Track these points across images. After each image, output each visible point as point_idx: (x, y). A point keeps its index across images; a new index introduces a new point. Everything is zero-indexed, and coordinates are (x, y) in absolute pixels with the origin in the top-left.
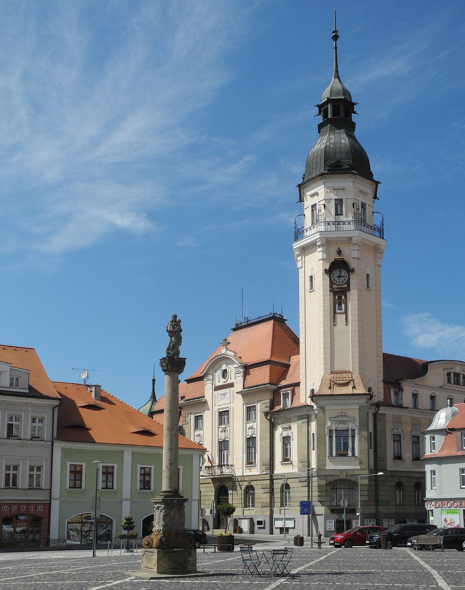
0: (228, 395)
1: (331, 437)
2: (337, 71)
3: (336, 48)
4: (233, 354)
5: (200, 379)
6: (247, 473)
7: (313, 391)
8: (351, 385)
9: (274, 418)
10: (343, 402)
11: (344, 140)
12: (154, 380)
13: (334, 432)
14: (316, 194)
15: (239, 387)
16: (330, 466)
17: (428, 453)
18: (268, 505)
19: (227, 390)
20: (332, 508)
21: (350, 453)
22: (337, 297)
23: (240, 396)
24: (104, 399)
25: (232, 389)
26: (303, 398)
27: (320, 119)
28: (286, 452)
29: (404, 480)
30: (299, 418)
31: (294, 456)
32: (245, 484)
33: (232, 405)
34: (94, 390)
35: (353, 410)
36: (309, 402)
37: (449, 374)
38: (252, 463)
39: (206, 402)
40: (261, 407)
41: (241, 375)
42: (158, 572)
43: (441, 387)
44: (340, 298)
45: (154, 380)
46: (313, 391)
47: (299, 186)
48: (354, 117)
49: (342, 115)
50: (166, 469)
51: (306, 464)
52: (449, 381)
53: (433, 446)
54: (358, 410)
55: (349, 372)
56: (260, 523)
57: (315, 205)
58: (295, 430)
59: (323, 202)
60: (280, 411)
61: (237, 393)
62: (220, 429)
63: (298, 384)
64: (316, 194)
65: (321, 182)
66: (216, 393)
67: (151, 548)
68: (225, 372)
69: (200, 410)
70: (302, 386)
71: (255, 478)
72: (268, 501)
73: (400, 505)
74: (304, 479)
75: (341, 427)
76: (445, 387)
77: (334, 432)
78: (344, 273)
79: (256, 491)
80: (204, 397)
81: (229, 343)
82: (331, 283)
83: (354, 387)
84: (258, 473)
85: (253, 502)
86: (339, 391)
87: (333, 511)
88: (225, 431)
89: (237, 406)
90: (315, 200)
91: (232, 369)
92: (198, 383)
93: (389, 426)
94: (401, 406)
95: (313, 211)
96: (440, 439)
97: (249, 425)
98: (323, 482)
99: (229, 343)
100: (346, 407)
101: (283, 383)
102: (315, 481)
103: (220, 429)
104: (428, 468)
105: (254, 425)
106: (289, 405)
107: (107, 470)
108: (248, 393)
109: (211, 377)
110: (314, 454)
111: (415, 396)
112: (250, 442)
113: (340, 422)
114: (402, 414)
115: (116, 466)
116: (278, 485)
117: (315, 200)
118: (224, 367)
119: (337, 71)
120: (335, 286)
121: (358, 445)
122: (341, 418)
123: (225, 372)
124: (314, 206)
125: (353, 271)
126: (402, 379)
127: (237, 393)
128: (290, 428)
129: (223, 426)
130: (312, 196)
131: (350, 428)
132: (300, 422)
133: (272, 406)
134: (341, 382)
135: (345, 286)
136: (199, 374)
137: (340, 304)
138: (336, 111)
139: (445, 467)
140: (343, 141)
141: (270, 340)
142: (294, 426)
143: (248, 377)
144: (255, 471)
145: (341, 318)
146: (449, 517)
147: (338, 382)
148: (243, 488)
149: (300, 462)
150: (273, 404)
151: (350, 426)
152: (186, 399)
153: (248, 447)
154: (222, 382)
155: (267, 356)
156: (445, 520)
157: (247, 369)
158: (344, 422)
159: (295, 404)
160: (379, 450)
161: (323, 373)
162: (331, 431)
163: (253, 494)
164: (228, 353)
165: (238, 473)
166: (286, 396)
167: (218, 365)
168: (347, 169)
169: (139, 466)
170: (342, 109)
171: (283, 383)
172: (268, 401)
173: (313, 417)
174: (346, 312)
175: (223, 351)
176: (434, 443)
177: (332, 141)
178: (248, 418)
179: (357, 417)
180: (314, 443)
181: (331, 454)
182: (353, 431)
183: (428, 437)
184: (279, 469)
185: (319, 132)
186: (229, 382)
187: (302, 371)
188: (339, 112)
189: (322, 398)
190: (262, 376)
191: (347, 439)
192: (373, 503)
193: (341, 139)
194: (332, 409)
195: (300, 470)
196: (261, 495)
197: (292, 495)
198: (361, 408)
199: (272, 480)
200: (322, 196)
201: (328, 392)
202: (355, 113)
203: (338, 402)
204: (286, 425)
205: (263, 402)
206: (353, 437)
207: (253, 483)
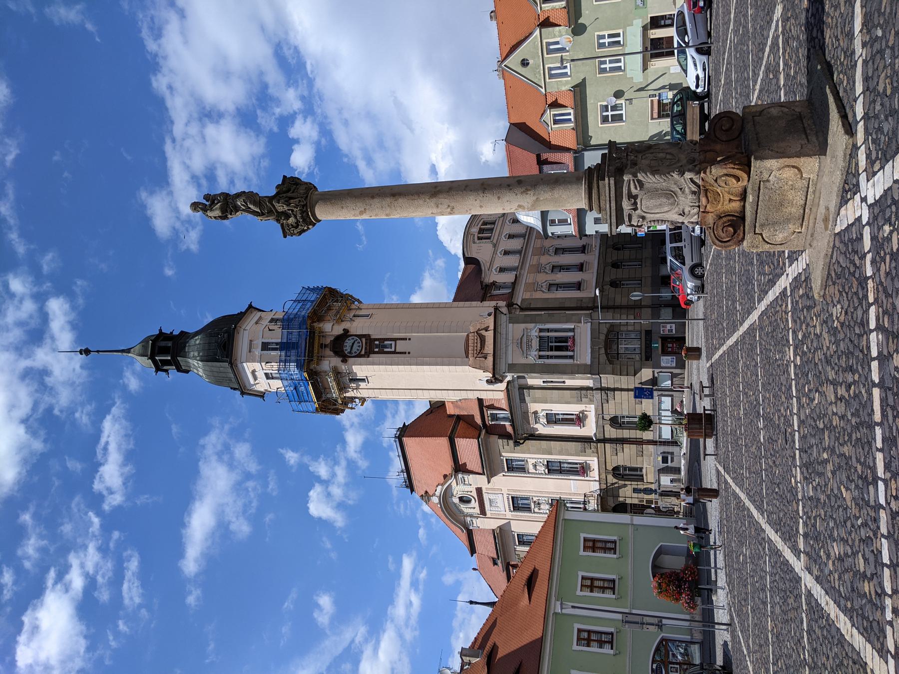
0: (492, 497)
1: (548, 357)
2: (123, 351)
3: (98, 351)
4: (440, 487)
5: (470, 534)
6: (595, 474)
7: (489, 382)
8: (483, 332)
9: (522, 435)
10: (504, 341)
11: (198, 340)
12: (471, 602)
13: (542, 353)
14: (253, 372)
15: (480, 481)
17: (571, 229)
18: (639, 447)
19: (486, 497)
20: (644, 358)
21: (571, 334)
22: (377, 350)
23: (493, 479)
24: (482, 647)
25: (484, 491)
26: (497, 394)
27: (172, 370)
28: (567, 420)
29: (607, 279)
30: (523, 400)
31: (574, 409)
32: (611, 479)
33: (505, 492)
34: (468, 658)
35: (514, 330)
36: (502, 386)
37: (479, 238)
38: (583, 467)
39: (500, 528)
40: (508, 452)
41: (466, 477)
42: (822, 149)
43: (495, 246)
44: (377, 346)
45: (471, 602)
46: (489, 382)
47: (243, 393)
48: (176, 333)
49: (170, 344)
50: (531, 192)
51: (583, 392)
52: (489, 238)
53: (563, 222)
54: (516, 325)
55: (468, 336)
56: (665, 460)
57: (266, 374)
58: (538, 407)
59: (263, 364)
60: (513, 426)
61: (489, 482)
62: (536, 510)
63: (480, 401)
64: (253, 372)
65: (239, 365)
66: (488, 514)
67: (742, 218)
68: (464, 500)
69: (511, 538)
70: (483, 395)
71: (603, 464)
72: (634, 447)
74: (604, 397)
75: (535, 343)
76: (495, 241)
77: (542, 353)
78: (348, 343)
79: (621, 463)
80: (493, 530)
81: (426, 492)
82: (359, 356)
83: (486, 329)
84: (596, 459)
85: (635, 469)
86: (489, 348)
87: (648, 357)
88: (539, 504)
89: (505, 485)
90: (260, 374)
91: (458, 490)
92: (477, 538)
93: (538, 295)
94: (514, 284)
95: (273, 378)
97: (531, 469)
98: (609, 367)
99: (426, 492)
100: (510, 338)
101: (478, 420)
102: (608, 380)
103: (536, 510)
105: (531, 462)
106: (506, 414)
107: (584, 639)
108: (490, 468)
109: (469, 519)
110: (570, 382)
111: (502, 270)
112: (554, 469)
113: (529, 347)
114: (524, 282)
115: (577, 626)
116: (612, 432)
117: (260, 374)
118: (456, 500)
119: (123, 351)
120: (363, 352)
121: (559, 326)
122: (523, 344)
123: (462, 499)
124: (268, 376)
125: (346, 331)
126: (482, 283)
127: (489, 482)
128: (536, 413)
129: (533, 506)
130: (255, 378)
131: (537, 334)
133: (507, 436)
134: (479, 345)
135: (364, 340)
136: (464, 536)
137: (386, 347)
138: (164, 351)
140: (198, 342)
141: (425, 439)
142: (533, 407)
143: (469, 467)
144: (594, 462)
145: (401, 346)
147: (479, 348)
148: (615, 480)
149: (580, 401)
150: (506, 436)
151: (535, 333)
152: (496, 557)
153: (561, 471)
154: (475, 504)
155: (444, 442)
157: (459, 468)
158: (529, 341)
159: (504, 404)
160: (567, 305)
161: (467, 367)
162: (540, 357)
163: (625, 468)
164: (437, 493)
165: (595, 486)
166: (494, 417)
167: (454, 509)
168: (229, 336)
169: (579, 593)
170: (163, 344)
171: (478, 420)
172: (500, 441)
173: (522, 381)
174: (395, 340)
175: (435, 500)
176: (560, 221)
177: (196, 354)
178: (522, 469)
179: (523, 326)
180: (556, 379)
181: (572, 357)
182: (541, 330)
183: (551, 230)
184: (590, 429)
185: (187, 372)
186: (475, 494)
187: (464, 395)
188: (166, 350)
189: (497, 366)
190: (468, 448)
191: (552, 337)
192: (637, 310)
194: (513, 356)
195: (591, 401)
196: (626, 456)
197: (625, 413)
198: (513, 321)
199: (604, 441)
200: (257, 366)
202: (172, 333)
204: (532, 419)
205: (501, 447)
206: (548, 330)
207: (610, 468)
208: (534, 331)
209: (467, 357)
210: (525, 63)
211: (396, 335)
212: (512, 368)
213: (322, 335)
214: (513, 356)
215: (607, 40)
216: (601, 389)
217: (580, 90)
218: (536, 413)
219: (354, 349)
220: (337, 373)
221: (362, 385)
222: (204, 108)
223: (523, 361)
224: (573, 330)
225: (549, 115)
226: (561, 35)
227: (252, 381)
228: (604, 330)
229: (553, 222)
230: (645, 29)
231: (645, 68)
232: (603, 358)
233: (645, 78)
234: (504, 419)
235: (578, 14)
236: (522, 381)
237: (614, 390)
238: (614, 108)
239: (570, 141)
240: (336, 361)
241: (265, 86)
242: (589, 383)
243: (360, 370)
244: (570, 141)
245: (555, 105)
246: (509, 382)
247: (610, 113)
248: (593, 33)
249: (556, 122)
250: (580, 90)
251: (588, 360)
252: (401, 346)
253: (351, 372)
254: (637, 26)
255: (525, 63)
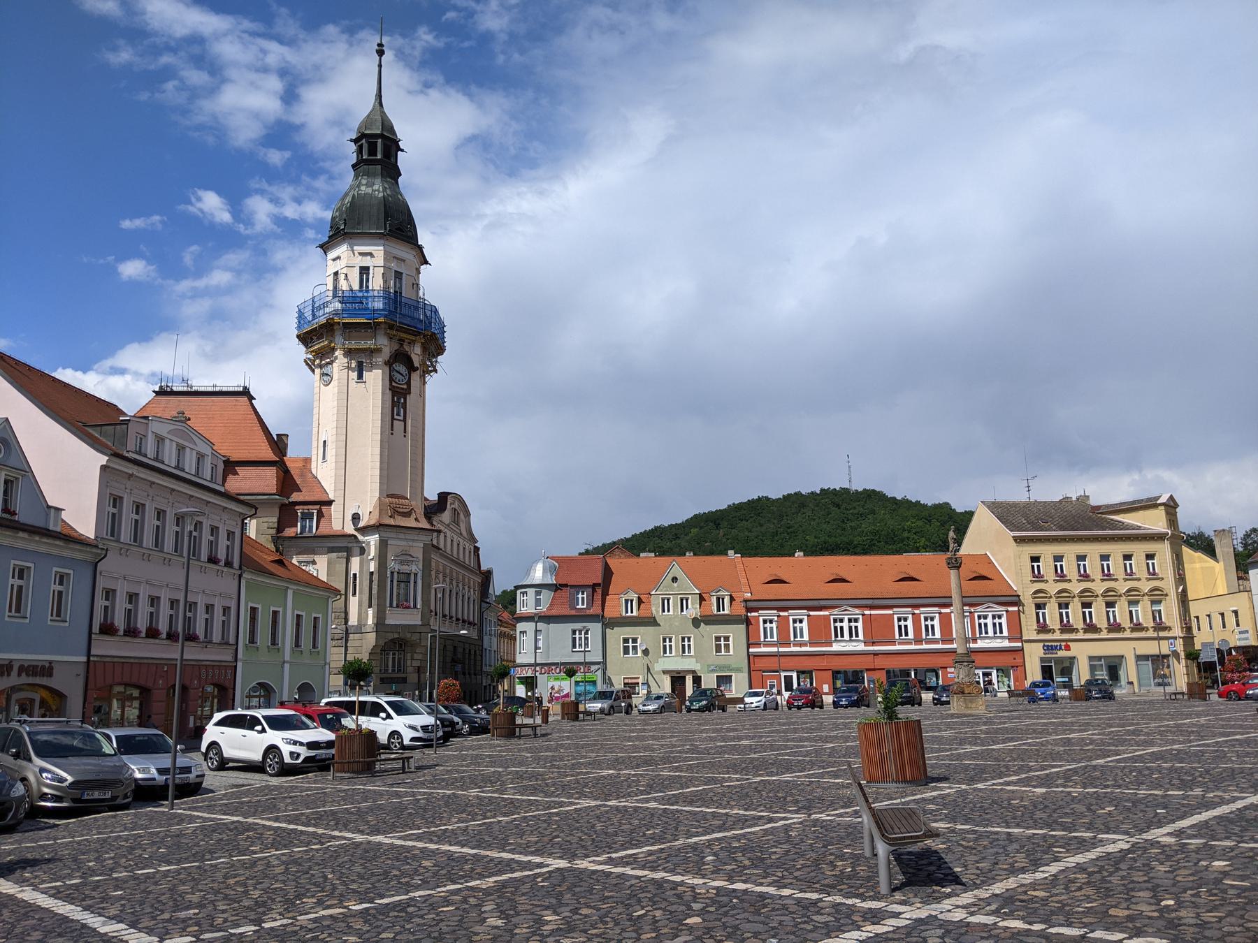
14: (371, 255)
16: (390, 620)
26: (339, 521)
44: (399, 399)
51: (343, 615)
57: (368, 268)
64: (371, 255)
73: (172, 636)
75: (405, 569)
82: (391, 379)
96: (546, 596)
98: (382, 643)
104: (521, 626)
113: (402, 562)
117: (367, 262)
132: (334, 555)
133: (280, 529)
139: (554, 627)
143: (231, 478)
145: (398, 425)
146: (557, 684)
151: (414, 568)
156: (552, 688)
158: (406, 563)
159: (324, 529)
162: (392, 573)
171: (295, 497)
174: (405, 420)
182: (416, 575)
193: (376, 188)
194: (395, 546)
201: (392, 522)
203: (402, 536)
205: (265, 519)
208: (416, 568)
209: (388, 496)
210: (674, 579)
211: (409, 422)
212: (383, 545)
213: (412, 343)
214: (395, 546)
215: (686, 643)
216: (347, 633)
217: (652, 622)
218: (314, 563)
219: (397, 375)
220: (372, 352)
221: (354, 375)
222: (307, 82)
223: (391, 556)
224: (415, 607)
225: (634, 597)
226: (693, 610)
227: (358, 249)
228: (415, 637)
229: (538, 593)
230: (694, 672)
231: (664, 672)
232: (390, 636)
233: (658, 672)
234: (303, 528)
235: (707, 623)
236: (357, 550)
237: (346, 647)
238: (635, 648)
239: (609, 613)
240: (386, 353)
241: (315, 174)
242: (353, 620)
243: (375, 378)
244: (609, 613)
245: (640, 601)
246: (355, 537)
247: (630, 644)
248: (693, 633)
249: (627, 601)
250: (652, 622)
251: (389, 621)
252: (398, 425)
253: (372, 367)
254: (696, 666)
255: (674, 579)
